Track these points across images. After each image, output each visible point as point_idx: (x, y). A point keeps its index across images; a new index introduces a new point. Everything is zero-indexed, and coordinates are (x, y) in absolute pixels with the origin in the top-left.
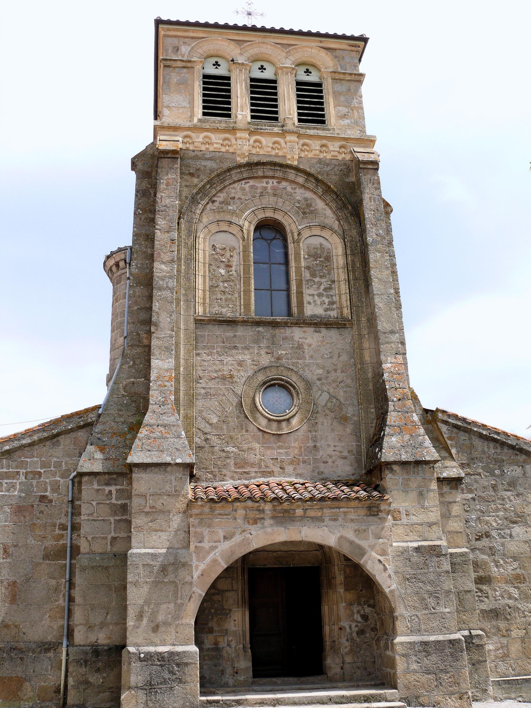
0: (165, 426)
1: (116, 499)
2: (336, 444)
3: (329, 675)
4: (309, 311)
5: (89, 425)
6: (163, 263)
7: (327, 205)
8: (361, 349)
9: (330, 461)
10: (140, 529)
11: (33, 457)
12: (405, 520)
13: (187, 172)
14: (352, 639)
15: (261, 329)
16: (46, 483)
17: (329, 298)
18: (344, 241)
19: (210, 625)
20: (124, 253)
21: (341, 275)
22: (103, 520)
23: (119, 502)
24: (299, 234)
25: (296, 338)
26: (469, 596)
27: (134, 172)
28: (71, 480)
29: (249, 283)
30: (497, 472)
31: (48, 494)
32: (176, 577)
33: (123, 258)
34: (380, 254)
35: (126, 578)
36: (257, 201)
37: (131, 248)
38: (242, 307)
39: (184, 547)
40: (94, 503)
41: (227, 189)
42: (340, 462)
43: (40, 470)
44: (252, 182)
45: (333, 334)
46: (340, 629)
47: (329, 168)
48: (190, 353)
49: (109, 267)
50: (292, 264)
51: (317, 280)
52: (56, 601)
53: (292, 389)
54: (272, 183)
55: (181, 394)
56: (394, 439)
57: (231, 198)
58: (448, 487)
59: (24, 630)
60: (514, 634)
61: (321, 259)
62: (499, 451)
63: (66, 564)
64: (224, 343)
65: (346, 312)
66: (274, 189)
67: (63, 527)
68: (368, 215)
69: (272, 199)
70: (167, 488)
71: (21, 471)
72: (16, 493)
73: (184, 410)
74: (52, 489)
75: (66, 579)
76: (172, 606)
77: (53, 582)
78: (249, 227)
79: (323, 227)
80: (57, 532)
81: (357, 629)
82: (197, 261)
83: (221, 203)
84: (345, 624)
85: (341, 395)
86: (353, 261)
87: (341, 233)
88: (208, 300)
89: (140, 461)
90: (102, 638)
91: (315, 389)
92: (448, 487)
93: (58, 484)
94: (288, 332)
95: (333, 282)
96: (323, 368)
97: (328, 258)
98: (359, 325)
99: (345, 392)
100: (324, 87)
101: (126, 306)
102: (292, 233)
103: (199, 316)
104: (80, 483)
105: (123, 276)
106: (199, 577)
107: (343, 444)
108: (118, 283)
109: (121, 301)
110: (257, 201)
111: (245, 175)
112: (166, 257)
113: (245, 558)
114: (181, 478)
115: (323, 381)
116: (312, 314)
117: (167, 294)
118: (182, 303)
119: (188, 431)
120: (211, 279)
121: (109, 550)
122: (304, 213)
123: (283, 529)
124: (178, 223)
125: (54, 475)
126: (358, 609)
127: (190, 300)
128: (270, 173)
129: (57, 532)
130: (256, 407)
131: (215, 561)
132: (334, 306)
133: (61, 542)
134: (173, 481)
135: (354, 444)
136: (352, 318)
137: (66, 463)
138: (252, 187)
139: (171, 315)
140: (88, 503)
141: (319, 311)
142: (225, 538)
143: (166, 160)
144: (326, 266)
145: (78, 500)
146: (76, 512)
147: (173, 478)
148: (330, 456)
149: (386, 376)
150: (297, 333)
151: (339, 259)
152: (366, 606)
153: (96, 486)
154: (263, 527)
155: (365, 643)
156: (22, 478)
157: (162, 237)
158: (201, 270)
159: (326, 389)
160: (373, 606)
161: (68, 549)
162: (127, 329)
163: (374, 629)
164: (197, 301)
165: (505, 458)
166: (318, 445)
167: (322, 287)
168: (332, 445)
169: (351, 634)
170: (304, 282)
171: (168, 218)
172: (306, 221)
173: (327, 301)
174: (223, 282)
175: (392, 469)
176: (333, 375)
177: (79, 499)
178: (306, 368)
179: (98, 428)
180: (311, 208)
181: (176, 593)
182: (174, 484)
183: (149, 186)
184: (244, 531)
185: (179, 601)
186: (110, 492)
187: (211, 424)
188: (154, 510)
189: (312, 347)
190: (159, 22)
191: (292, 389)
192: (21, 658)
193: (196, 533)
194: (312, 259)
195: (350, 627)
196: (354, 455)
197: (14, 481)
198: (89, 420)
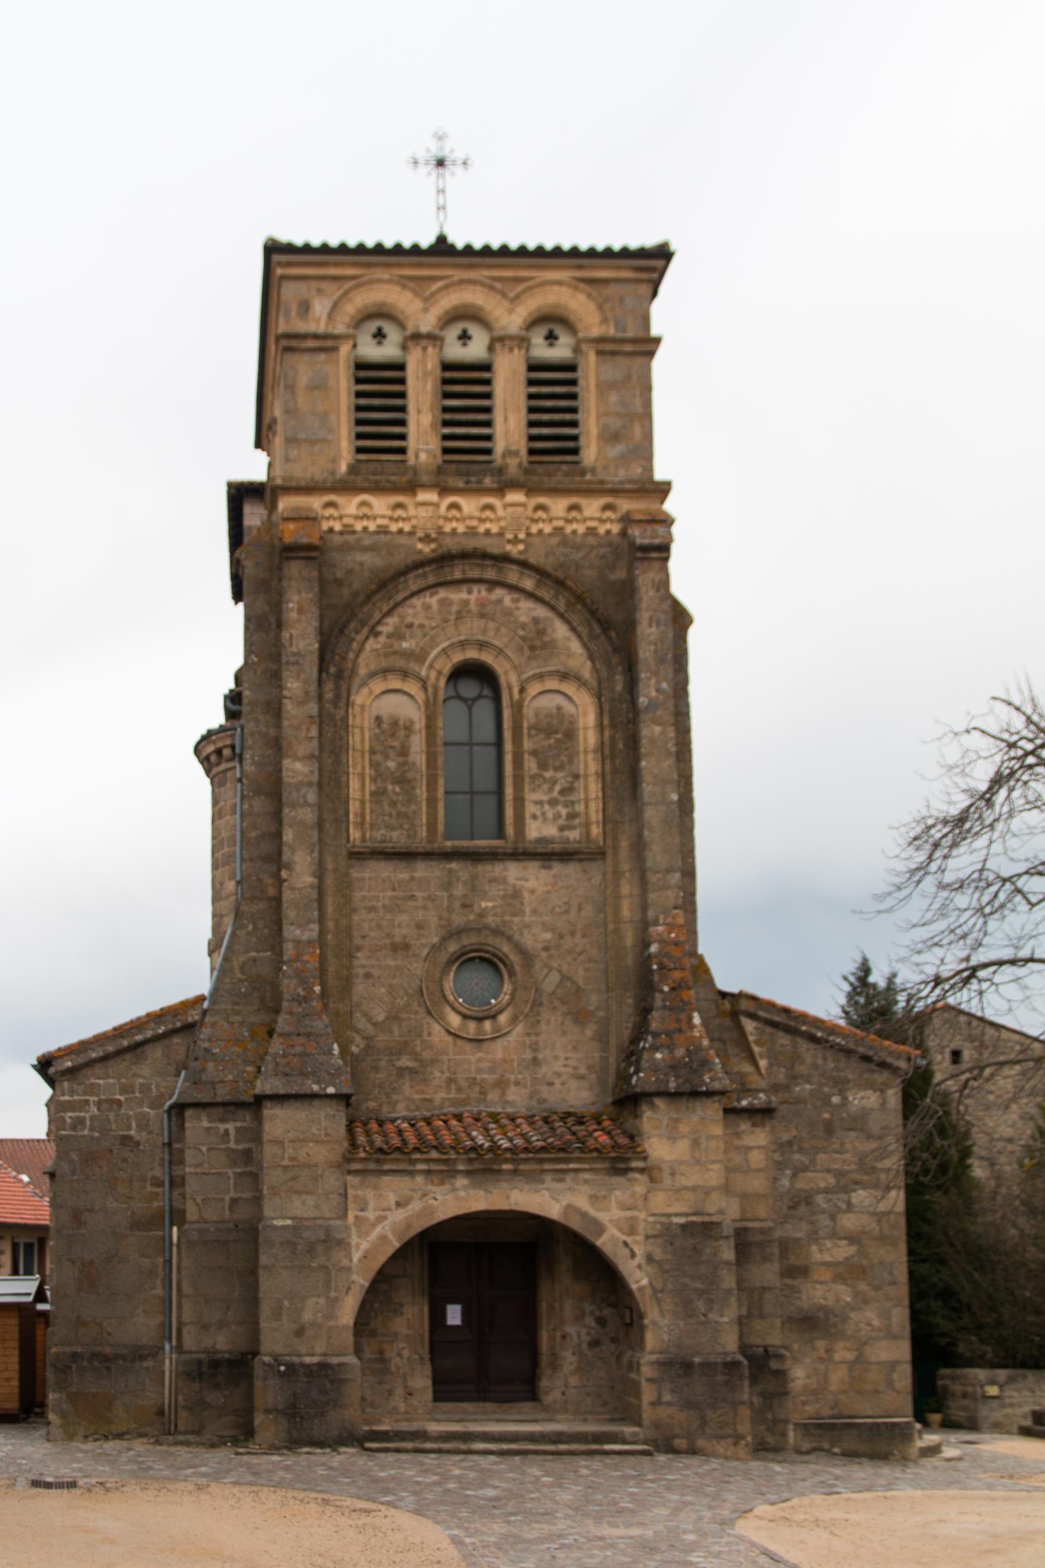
0: (308, 1035)
1: (237, 1141)
2: (569, 1055)
4: (534, 830)
5: (189, 1028)
6: (299, 759)
7: (573, 629)
8: (617, 897)
9: (557, 1081)
10: (275, 1192)
11: (109, 1077)
12: (667, 1181)
14: (581, 1352)
15: (454, 865)
16: (128, 1117)
19: (372, 1326)
21: (590, 765)
23: (240, 1147)
24: (522, 690)
25: (511, 879)
29: (436, 784)
31: (132, 1133)
32: (328, 1260)
35: (257, 1259)
36: (450, 629)
39: (338, 1218)
40: (204, 1149)
41: (400, 610)
42: (573, 1084)
43: (118, 1097)
44: (442, 593)
45: (572, 870)
47: (580, 554)
50: (508, 746)
51: (549, 774)
52: (153, 1288)
53: (502, 966)
54: (476, 594)
56: (659, 1056)
59: (109, 1330)
60: (838, 1357)
62: (842, 1065)
64: (394, 890)
65: (596, 831)
66: (482, 604)
67: (157, 1183)
68: (645, 653)
69: (478, 623)
70: (314, 1130)
72: (86, 1132)
74: (138, 1126)
76: (322, 1300)
77: (146, 1262)
78: (437, 679)
79: (564, 676)
83: (390, 636)
85: (580, 975)
86: (612, 738)
87: (595, 684)
88: (368, 818)
90: (222, 1342)
91: (538, 966)
94: (497, 869)
95: (576, 777)
96: (553, 929)
97: (570, 734)
98: (615, 855)
99: (587, 970)
100: (579, 374)
102: (510, 688)
103: (354, 846)
105: (229, 774)
106: (360, 1261)
107: (579, 1055)
109: (228, 817)
110: (450, 629)
111: (431, 580)
112: (302, 750)
113: (423, 1235)
115: (553, 952)
120: (374, 780)
122: (532, 648)
123: (482, 1192)
125: (140, 1104)
128: (475, 573)
129: (149, 1189)
130: (444, 996)
131: (383, 1238)
132: (577, 822)
133: (156, 1204)
137: (157, 1086)
138: (443, 602)
141: (551, 831)
142: (398, 1204)
147: (322, 1114)
148: (558, 1075)
150: (513, 872)
151: (588, 736)
153: (205, 1123)
154: (454, 1190)
156: (94, 1110)
157: (293, 712)
161: (167, 1215)
165: (851, 1077)
166: (540, 1056)
167: (558, 788)
168: (562, 1056)
169: (579, 1345)
170: (527, 780)
172: (534, 663)
173: (564, 812)
174: (394, 783)
178: (525, 931)
179: (205, 1032)
181: (327, 1283)
183: (267, 608)
184: (425, 1195)
185: (333, 1294)
186: (227, 1131)
187: (374, 1024)
190: (273, 250)
191: (502, 966)
193: (356, 1197)
194: (542, 736)
195: (579, 1336)
197: (82, 1114)
198: (190, 1020)
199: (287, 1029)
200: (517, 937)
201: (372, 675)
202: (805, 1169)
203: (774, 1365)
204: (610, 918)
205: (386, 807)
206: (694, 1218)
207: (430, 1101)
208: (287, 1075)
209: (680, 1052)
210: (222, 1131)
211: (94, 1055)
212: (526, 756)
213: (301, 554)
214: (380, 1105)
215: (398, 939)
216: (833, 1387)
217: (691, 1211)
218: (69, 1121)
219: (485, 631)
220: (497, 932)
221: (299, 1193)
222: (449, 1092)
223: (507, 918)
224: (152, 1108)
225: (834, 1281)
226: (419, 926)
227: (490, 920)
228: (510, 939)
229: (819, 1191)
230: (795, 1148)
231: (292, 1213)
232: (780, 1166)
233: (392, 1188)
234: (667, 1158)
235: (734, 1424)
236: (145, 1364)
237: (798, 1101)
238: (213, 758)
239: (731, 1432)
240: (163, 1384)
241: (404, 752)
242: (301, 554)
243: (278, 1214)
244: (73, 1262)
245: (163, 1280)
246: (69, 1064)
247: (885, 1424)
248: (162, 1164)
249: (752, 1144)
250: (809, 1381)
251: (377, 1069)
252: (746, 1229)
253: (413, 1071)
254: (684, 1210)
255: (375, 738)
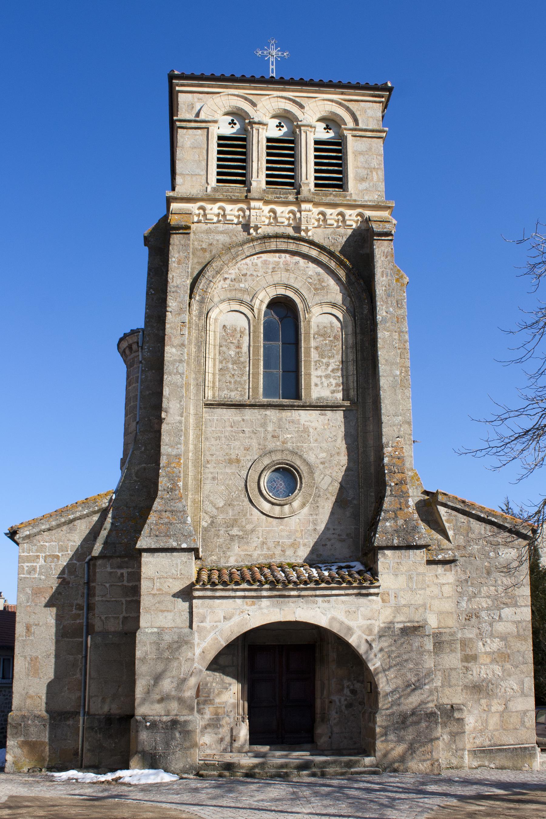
0: (172, 512)
1: (128, 581)
3: (319, 744)
6: (173, 346)
9: (329, 543)
13: (200, 247)
14: (341, 711)
17: (336, 379)
18: (355, 319)
20: (137, 336)
22: (116, 601)
23: (130, 584)
25: (302, 422)
26: (454, 673)
27: (147, 248)
28: (86, 562)
29: (258, 365)
30: (492, 554)
33: (136, 340)
34: (388, 333)
37: (143, 330)
38: (251, 390)
40: (107, 585)
43: (58, 554)
44: (264, 256)
46: (331, 702)
48: (199, 438)
49: (123, 349)
51: (325, 361)
52: (74, 675)
55: (190, 479)
56: (388, 524)
57: (243, 275)
58: (443, 569)
60: (493, 709)
61: (330, 339)
63: (82, 641)
64: (232, 427)
66: (286, 264)
67: (80, 608)
69: (285, 274)
71: (41, 554)
72: (36, 576)
73: (192, 495)
75: (82, 655)
77: (71, 658)
78: (260, 305)
80: (74, 611)
81: (346, 702)
82: (208, 343)
84: (335, 698)
88: (217, 384)
89: (384, 354)
92: (443, 569)
93: (74, 567)
101: (139, 391)
104: (95, 565)
108: (131, 366)
109: (134, 385)
111: (258, 250)
112: (176, 341)
114: (186, 562)
115: (326, 465)
116: (319, 396)
117: (177, 379)
118: (192, 387)
119: (196, 515)
120: (221, 362)
121: (120, 629)
122: (316, 289)
124: (190, 303)
126: (348, 684)
127: (202, 385)
128: (283, 247)
129: (74, 611)
133: (78, 621)
134: (179, 564)
135: (353, 527)
136: (357, 400)
139: (181, 401)
140: (102, 585)
142: (225, 618)
143: (178, 236)
144: (335, 346)
145: (93, 582)
146: (90, 593)
148: (330, 540)
149: (386, 460)
152: (355, 682)
153: (109, 569)
154: (261, 608)
155: (353, 715)
156: (42, 561)
157: (173, 320)
158: (212, 352)
159: (328, 473)
160: (362, 682)
161: (85, 627)
162: (140, 415)
163: (362, 703)
164: (207, 385)
167: (330, 368)
170: (313, 363)
171: (178, 299)
175: (384, 554)
176: (337, 458)
177: (94, 581)
180: (323, 284)
182: (179, 568)
183: (162, 264)
184: (242, 612)
186: (122, 574)
187: (217, 509)
188: (161, 592)
189: (318, 430)
192: (44, 725)
196: (352, 538)
199: (159, 508)
200: (305, 456)
201: (223, 301)
202: (475, 596)
203: (457, 715)
204: (360, 445)
205: (228, 378)
206: (409, 624)
207: (251, 556)
208: (157, 536)
209: (400, 522)
210: (119, 574)
211: (43, 527)
212: (312, 350)
213: (181, 231)
214: (219, 559)
215: (234, 457)
216: (491, 728)
217: (407, 620)
218: (26, 568)
219: (288, 279)
220: (293, 453)
221: (162, 611)
222: (262, 550)
223: (299, 444)
224: (78, 561)
225: (491, 663)
226: (247, 449)
227: (289, 445)
228: (301, 457)
229: (483, 609)
230: (469, 583)
231: (158, 625)
232: (461, 594)
233: (222, 607)
234: (392, 587)
235: (431, 752)
236: (68, 723)
237: (471, 555)
238: (127, 352)
239: (429, 757)
240: (79, 736)
241: (239, 347)
242: (181, 231)
243: (149, 625)
244: (25, 658)
245: (81, 670)
246: (28, 533)
247: (520, 748)
248: (82, 596)
249: (444, 582)
250: (477, 724)
251: (218, 536)
252: (440, 633)
253: (240, 538)
254: (404, 620)
255: (223, 338)
